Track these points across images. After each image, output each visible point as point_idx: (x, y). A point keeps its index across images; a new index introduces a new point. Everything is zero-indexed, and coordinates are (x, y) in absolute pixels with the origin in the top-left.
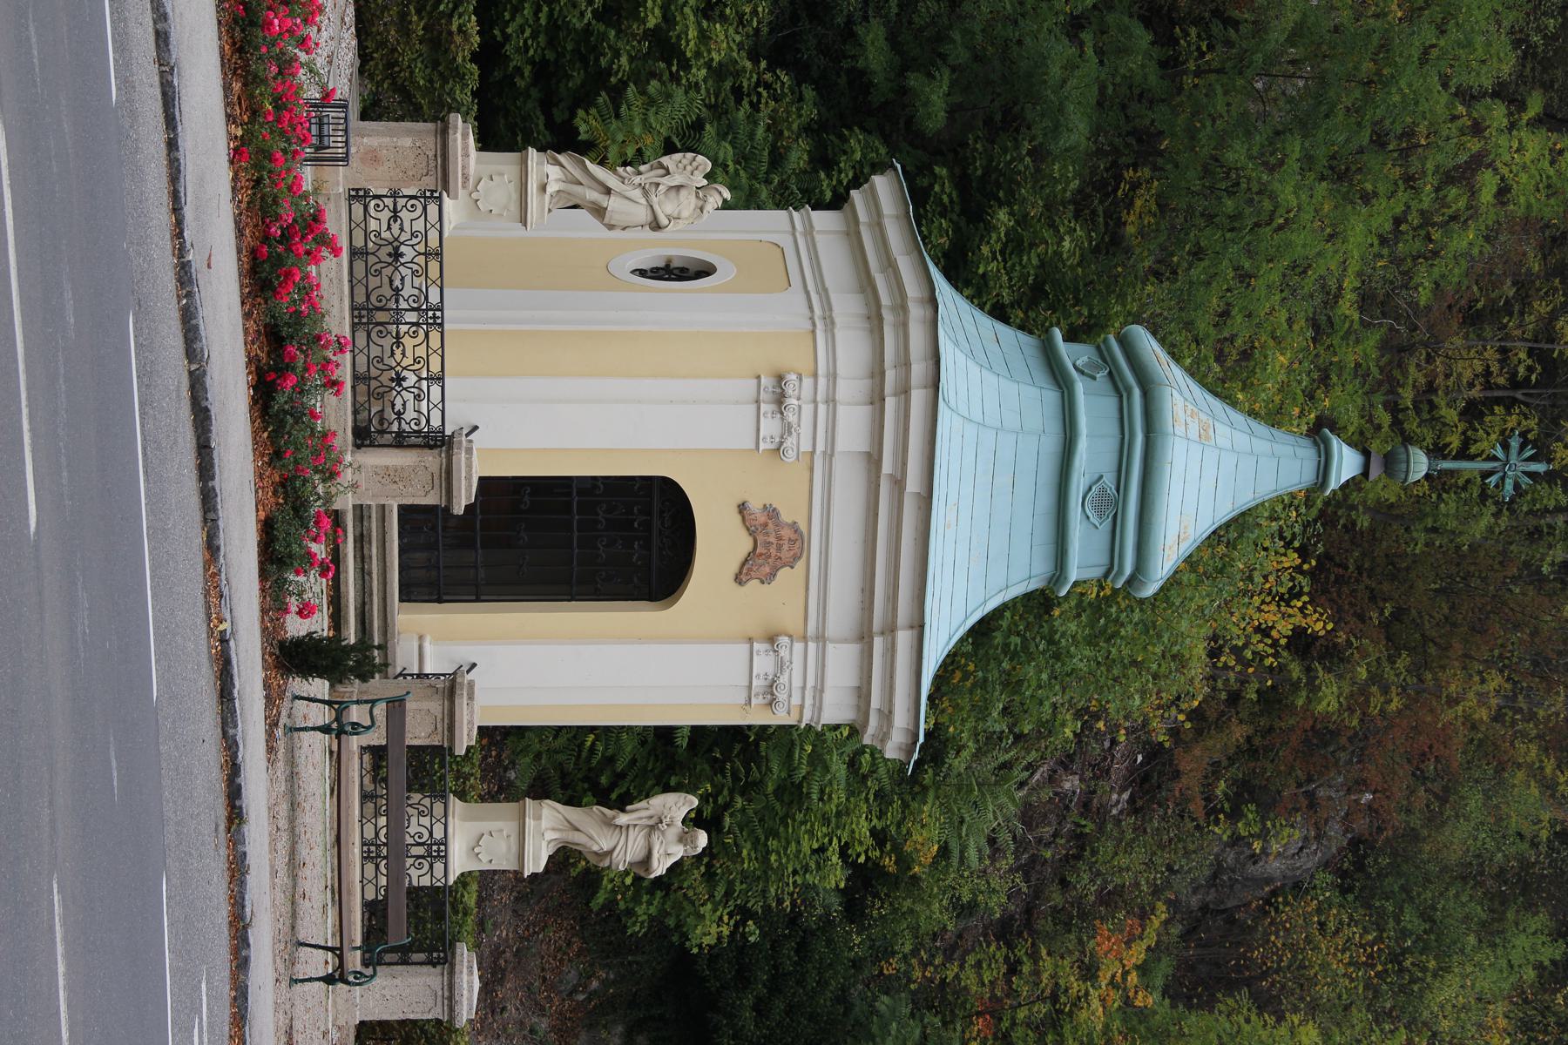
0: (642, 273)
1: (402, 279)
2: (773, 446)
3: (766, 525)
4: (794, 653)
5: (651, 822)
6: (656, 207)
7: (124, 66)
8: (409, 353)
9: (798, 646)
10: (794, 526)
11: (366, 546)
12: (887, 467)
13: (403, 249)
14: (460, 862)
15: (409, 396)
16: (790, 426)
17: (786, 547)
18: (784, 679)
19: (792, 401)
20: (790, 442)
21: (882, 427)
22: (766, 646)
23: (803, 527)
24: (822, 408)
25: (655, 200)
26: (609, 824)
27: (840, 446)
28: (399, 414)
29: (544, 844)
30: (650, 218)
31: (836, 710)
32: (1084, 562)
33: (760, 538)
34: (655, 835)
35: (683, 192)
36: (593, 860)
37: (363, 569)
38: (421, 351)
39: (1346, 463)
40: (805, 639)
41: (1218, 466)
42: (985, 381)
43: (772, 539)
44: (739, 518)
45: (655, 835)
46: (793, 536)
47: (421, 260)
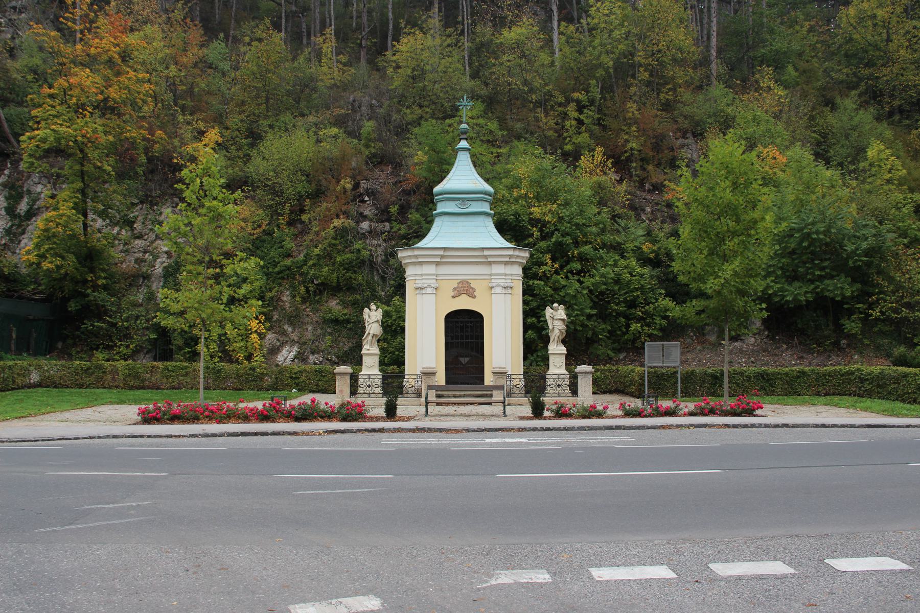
4: (495, 282)
7: (192, 445)
12: (438, 260)
14: (376, 371)
19: (420, 285)
31: (518, 271)
32: (486, 208)
34: (556, 317)
41: (463, 176)
42: (441, 235)
45: (556, 317)
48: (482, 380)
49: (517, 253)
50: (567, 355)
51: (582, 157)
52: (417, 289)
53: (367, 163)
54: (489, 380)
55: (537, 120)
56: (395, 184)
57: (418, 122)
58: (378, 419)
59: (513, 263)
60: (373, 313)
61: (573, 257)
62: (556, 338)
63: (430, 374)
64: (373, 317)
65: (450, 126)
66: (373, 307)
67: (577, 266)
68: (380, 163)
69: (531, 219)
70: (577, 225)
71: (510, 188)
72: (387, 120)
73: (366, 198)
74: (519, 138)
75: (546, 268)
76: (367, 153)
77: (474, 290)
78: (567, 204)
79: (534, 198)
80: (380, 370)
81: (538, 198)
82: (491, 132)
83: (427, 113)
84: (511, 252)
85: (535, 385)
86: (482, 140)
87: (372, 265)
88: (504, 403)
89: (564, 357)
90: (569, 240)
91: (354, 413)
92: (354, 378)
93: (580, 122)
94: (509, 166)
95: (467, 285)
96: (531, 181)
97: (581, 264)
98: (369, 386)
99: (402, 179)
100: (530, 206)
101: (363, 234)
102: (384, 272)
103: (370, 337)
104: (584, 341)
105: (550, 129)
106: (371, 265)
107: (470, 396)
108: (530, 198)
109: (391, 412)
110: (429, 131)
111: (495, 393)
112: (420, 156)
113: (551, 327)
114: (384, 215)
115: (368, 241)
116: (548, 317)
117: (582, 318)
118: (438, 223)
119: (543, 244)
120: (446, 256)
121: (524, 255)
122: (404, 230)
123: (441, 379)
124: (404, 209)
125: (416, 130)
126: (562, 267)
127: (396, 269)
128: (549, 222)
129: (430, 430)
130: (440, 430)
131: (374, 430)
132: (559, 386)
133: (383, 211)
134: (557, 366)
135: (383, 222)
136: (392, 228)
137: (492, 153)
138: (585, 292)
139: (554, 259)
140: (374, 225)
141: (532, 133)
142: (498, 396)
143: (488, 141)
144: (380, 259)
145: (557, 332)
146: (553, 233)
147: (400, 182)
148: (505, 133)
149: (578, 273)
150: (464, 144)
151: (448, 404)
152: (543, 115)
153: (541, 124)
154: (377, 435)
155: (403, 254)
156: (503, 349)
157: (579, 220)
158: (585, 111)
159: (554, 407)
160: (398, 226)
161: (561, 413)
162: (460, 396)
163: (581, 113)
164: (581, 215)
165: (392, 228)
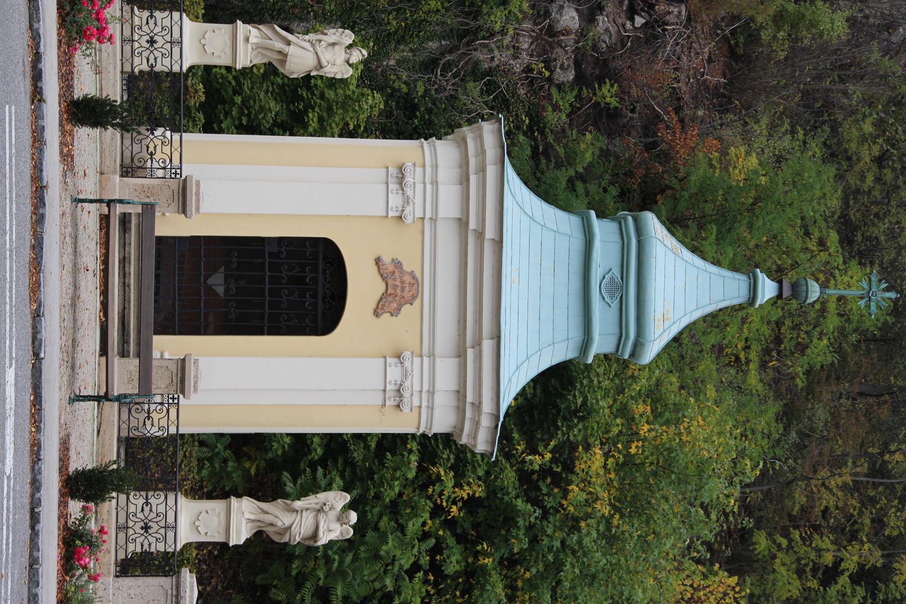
1: (156, 59)
2: (397, 214)
3: (393, 273)
5: (318, 507)
6: (319, 53)
8: (159, 23)
9: (417, 360)
10: (412, 274)
11: (127, 265)
12: (472, 225)
13: (156, 38)
15: (158, 143)
16: (408, 198)
17: (407, 289)
18: (407, 383)
19: (409, 179)
20: (409, 209)
21: (468, 198)
22: (396, 360)
24: (429, 187)
25: (319, 50)
27: (438, 387)
28: (151, 154)
29: (244, 522)
30: (315, 62)
31: (441, 424)
32: (602, 344)
33: (390, 282)
34: (322, 518)
35: (337, 47)
36: (276, 538)
37: (124, 283)
38: (162, 509)
39: (767, 289)
40: (421, 356)
41: (683, 286)
42: (536, 233)
43: (398, 283)
44: (376, 268)
45: (322, 518)
46: (412, 281)
47: (162, 531)
48: (165, 328)
49: (486, 422)
50: (224, 546)
51: (733, 580)
52: (401, 169)
53: (734, 18)
54: (167, 347)
55: (837, 463)
56: (676, 97)
57: (835, 153)
58: (67, 78)
59: (461, 411)
60: (340, 55)
61: (476, 554)
62: (269, 518)
63: (183, 200)
64: (329, 53)
65: (822, 243)
66: (357, 56)
67: (453, 563)
68: (732, 53)
69: (573, 447)
70: (558, 566)
71: (654, 395)
72: (847, 68)
73: (639, 21)
74: (788, 416)
75: (450, 484)
76: (760, 19)
77: (395, 313)
78: (610, 539)
79: (628, 455)
81: (628, 464)
82: (802, 348)
83: (863, 177)
84: (487, 406)
85: (153, 464)
86: (779, 323)
87: (466, 36)
88: (106, 397)
89: (219, 538)
90: (519, 543)
91: (80, 17)
93: (830, 575)
94: (711, 393)
95: (407, 295)
96: (670, 450)
97: (457, 574)
98: (152, 42)
99: (688, 112)
100: (608, 444)
101: (547, 14)
102: (447, 67)
103: (279, 45)
104: (259, 580)
105: (811, 497)
106: (466, 33)
107: (125, 300)
108: (627, 446)
109: (85, 112)
110: (809, 187)
111: (133, 363)
112: (746, 163)
113: (298, 504)
114: (594, 67)
115: (527, 25)
116: (322, 496)
117: (321, 574)
118: (560, 223)
119: (509, 477)
120: (480, 243)
121: (481, 440)
122: (554, 118)
123: (170, 225)
124: (606, 120)
125: (815, 148)
126: (451, 524)
127: (453, 98)
128: (565, 493)
129: (38, 220)
130: (38, 246)
131: (37, 76)
132: (146, 528)
133: (605, 64)
134: (196, 520)
135: (577, 65)
136: (559, 87)
137: (747, 348)
138: (389, 582)
139: (471, 504)
140: (570, 40)
141: (800, 448)
142: (124, 375)
143: (778, 340)
144: (480, 55)
145: (285, 519)
146: (536, 502)
147: (678, 110)
148: (800, 383)
149: (436, 568)
150: (767, 289)
151: (105, 244)
152: (848, 479)
153: (824, 473)
154: (24, 86)
155: (488, 135)
156: (246, 382)
157: (570, 571)
158: (861, 591)
159: (92, 526)
160: (565, 106)
161: (75, 544)
162: (124, 274)
163: (855, 579)
164: (583, 575)
165: (559, 87)
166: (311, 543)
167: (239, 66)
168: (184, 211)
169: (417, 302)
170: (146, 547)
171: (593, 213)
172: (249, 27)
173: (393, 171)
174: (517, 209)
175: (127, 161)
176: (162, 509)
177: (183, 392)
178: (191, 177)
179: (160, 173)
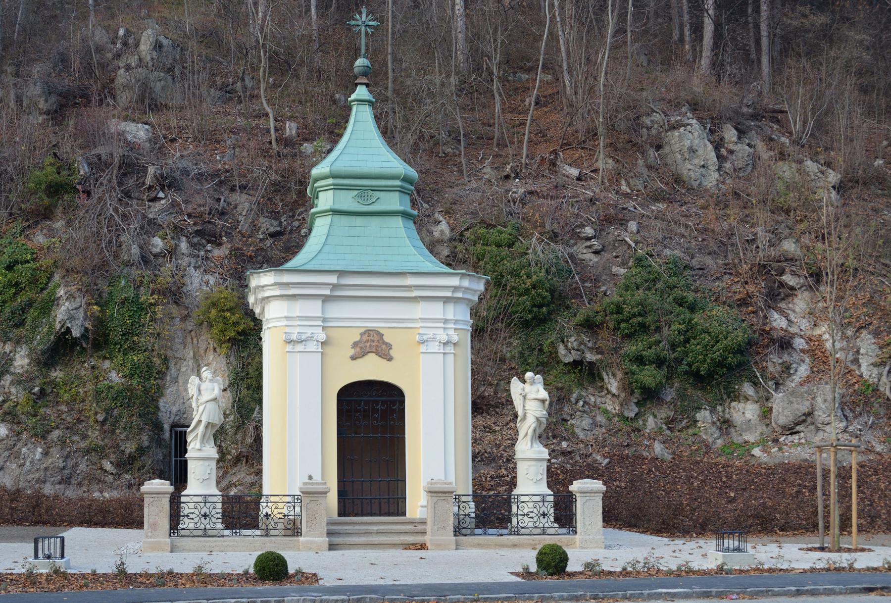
0: (511, 573)
8: (192, 511)
10: (362, 334)
12: (327, 292)
23: (363, 330)
26: (524, 417)
31: (463, 314)
32: (394, 202)
33: (368, 350)
36: (544, 426)
39: (361, 92)
43: (368, 344)
47: (208, 505)
52: (289, 342)
59: (456, 300)
77: (389, 346)
80: (549, 487)
92: (175, 501)
95: (376, 338)
103: (201, 428)
156: (435, 450)
166: (547, 403)
167: (217, 456)
168: (326, 493)
169: (381, 331)
170: (219, 516)
171: (312, 211)
172: (189, 448)
173: (289, 348)
174: (313, 262)
175: (289, 532)
176: (191, 505)
177: (452, 492)
178: (301, 488)
179: (298, 509)
